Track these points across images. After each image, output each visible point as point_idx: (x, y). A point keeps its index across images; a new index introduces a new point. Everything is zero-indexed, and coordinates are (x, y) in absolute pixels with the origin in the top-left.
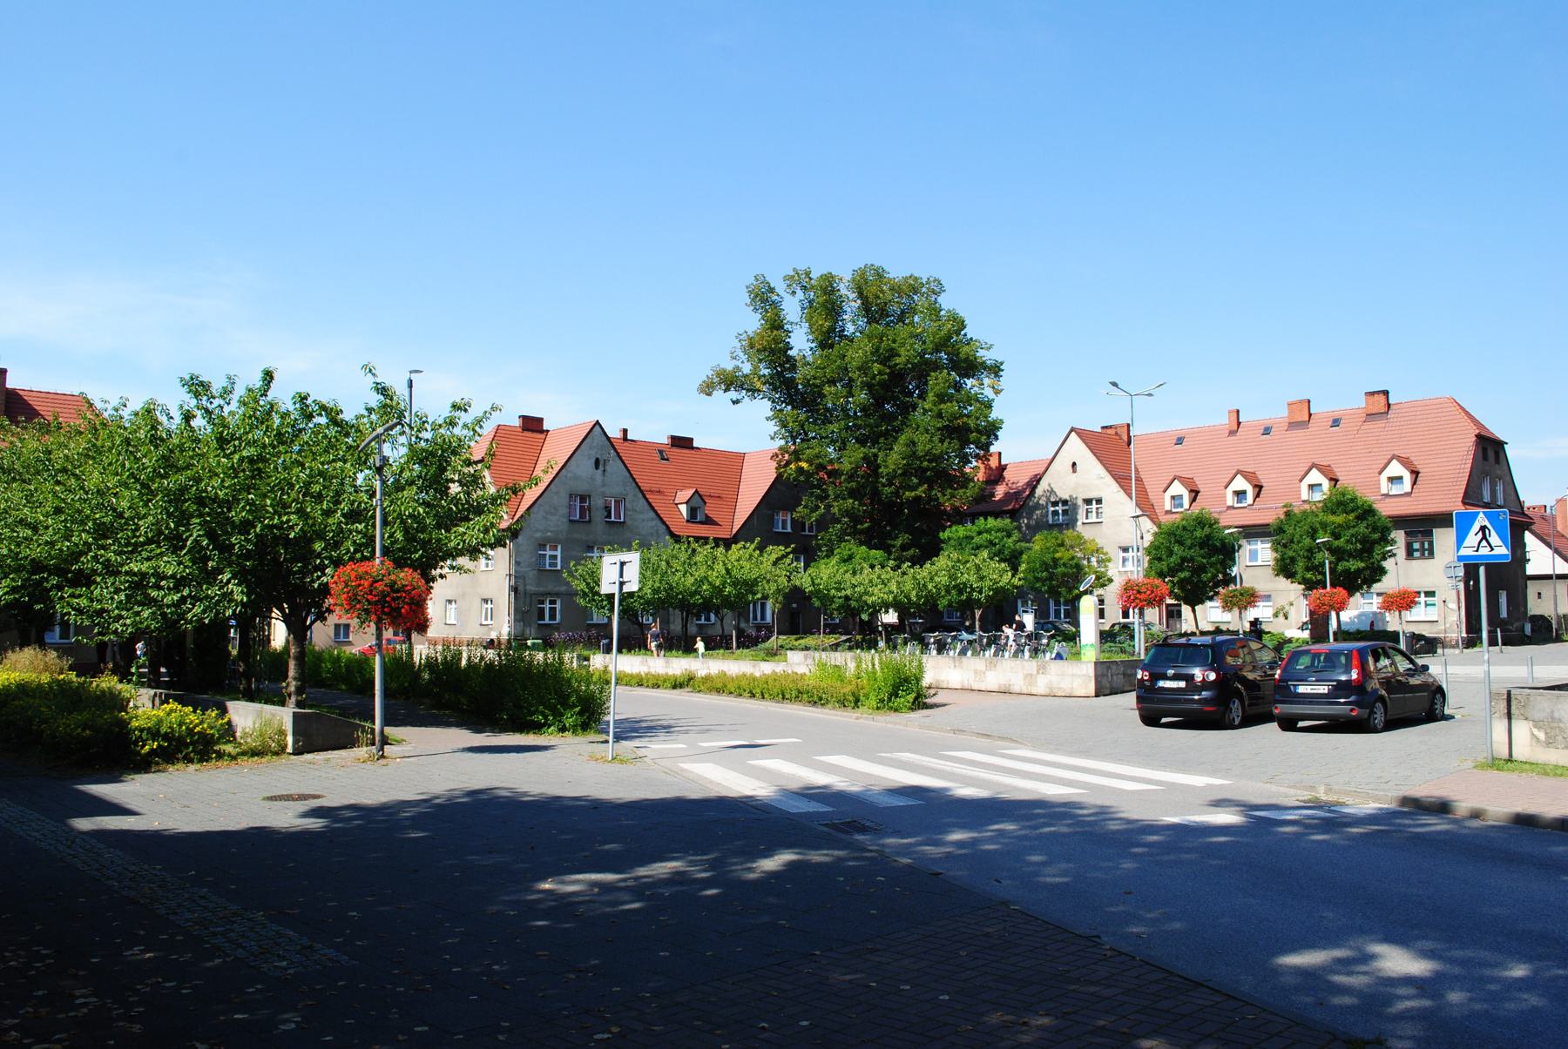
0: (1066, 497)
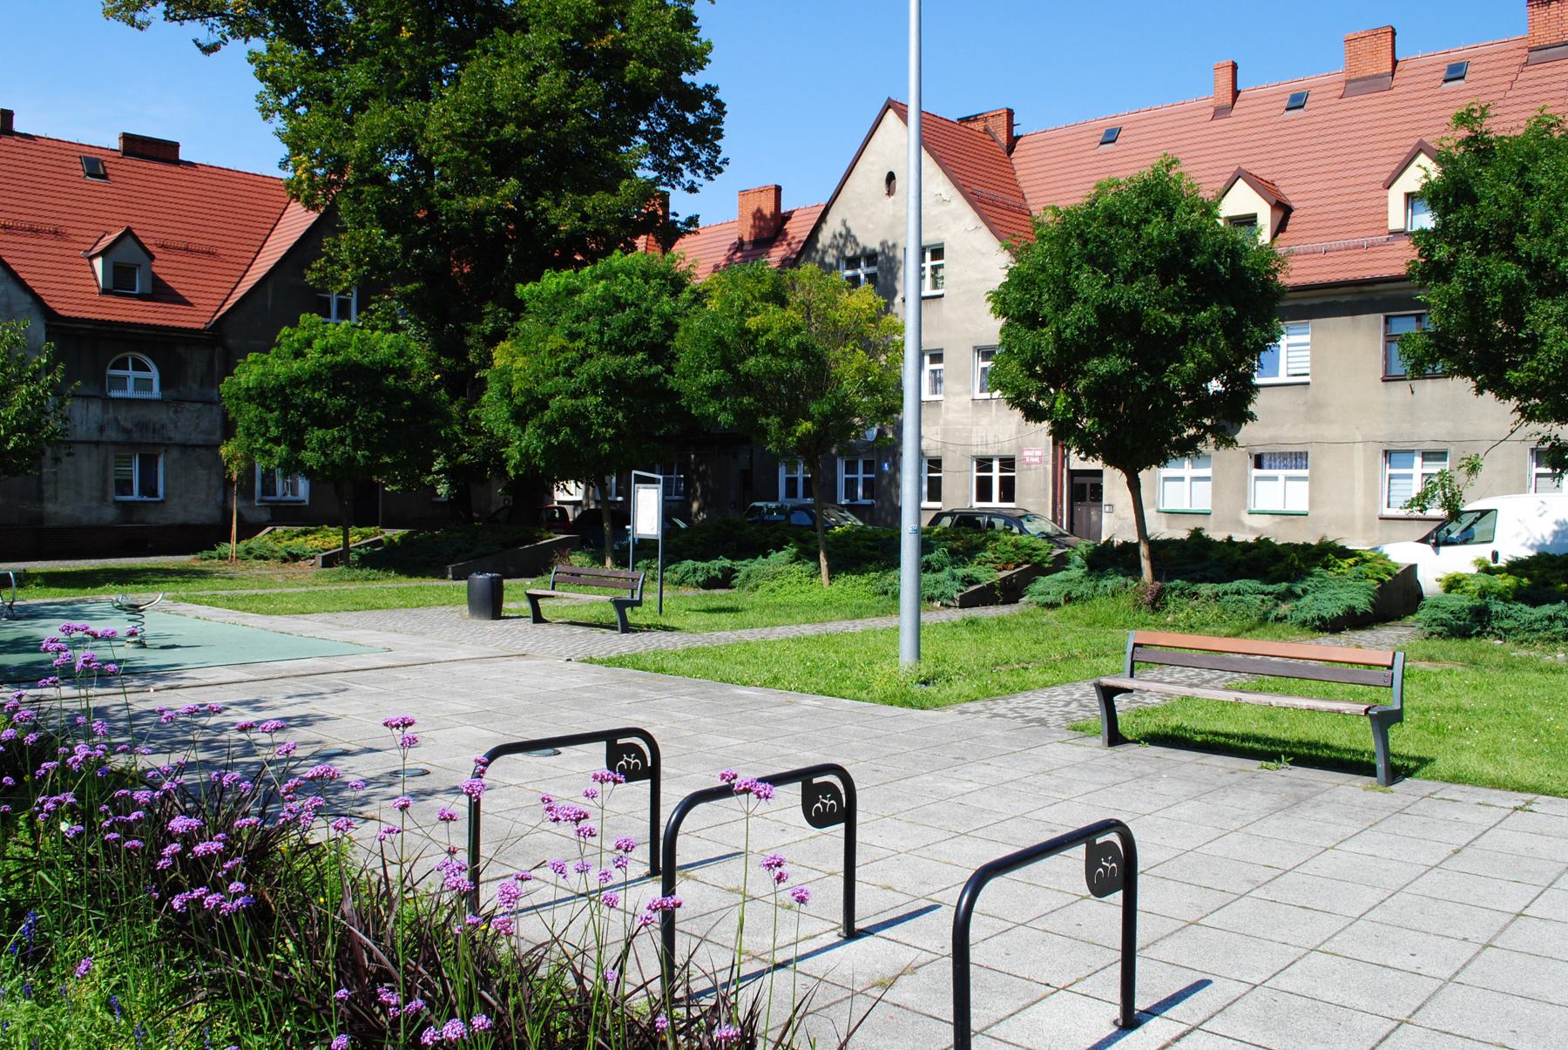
0: (873, 244)
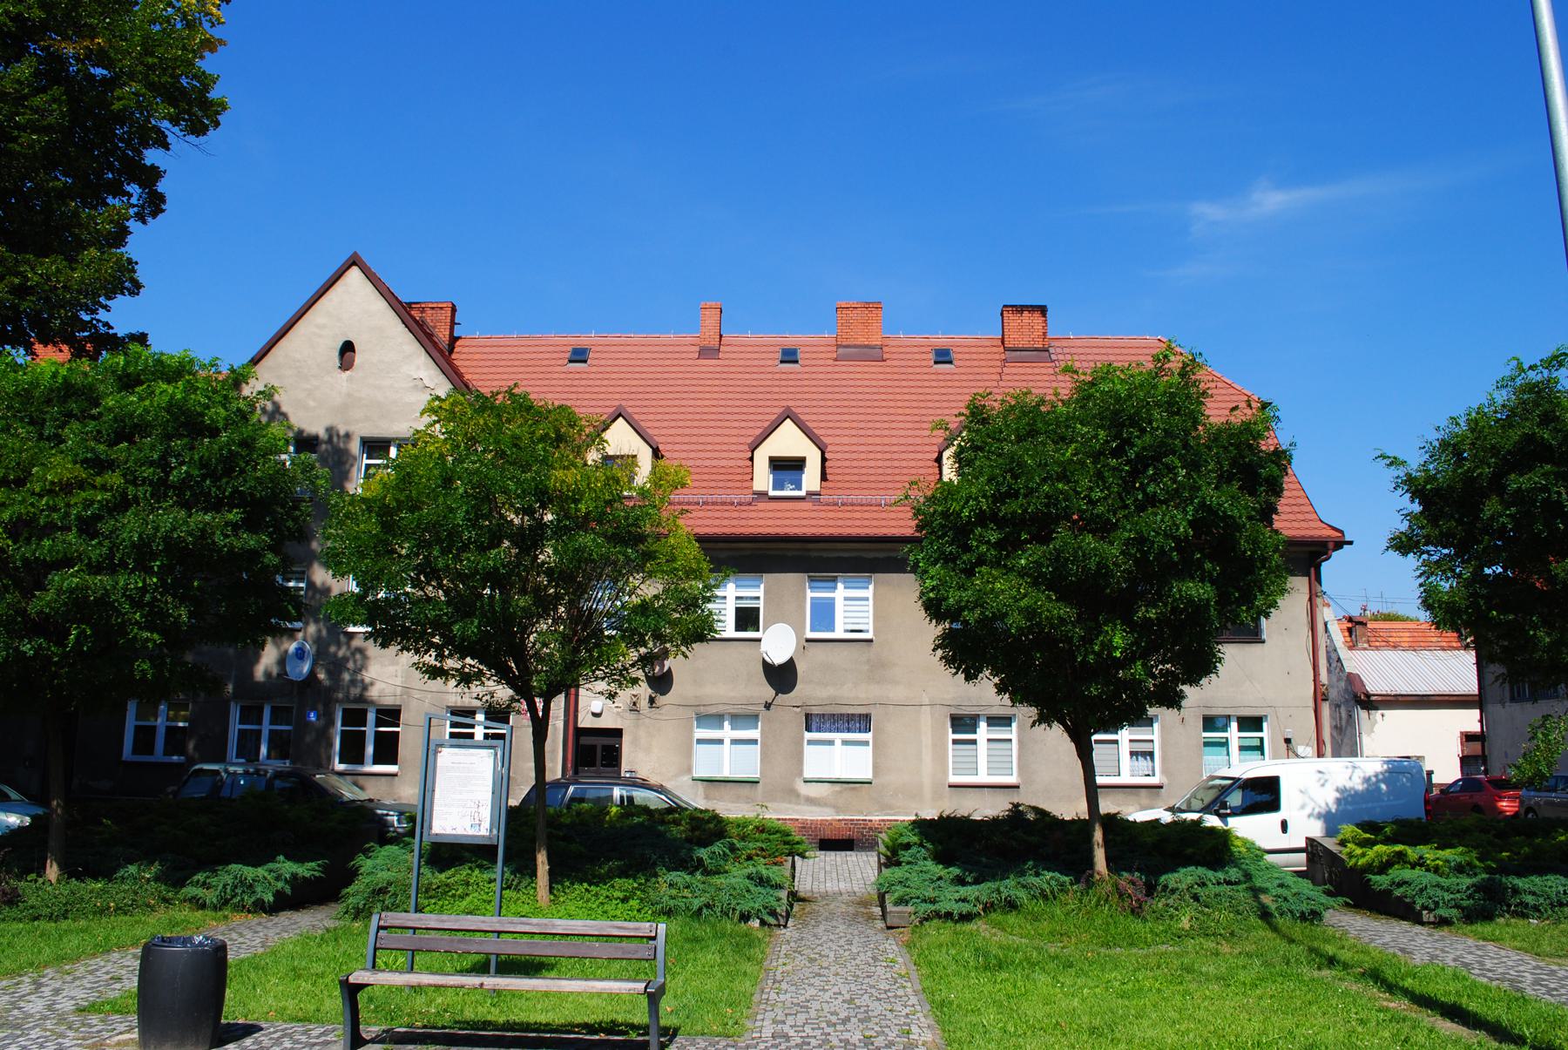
0: (316, 428)
